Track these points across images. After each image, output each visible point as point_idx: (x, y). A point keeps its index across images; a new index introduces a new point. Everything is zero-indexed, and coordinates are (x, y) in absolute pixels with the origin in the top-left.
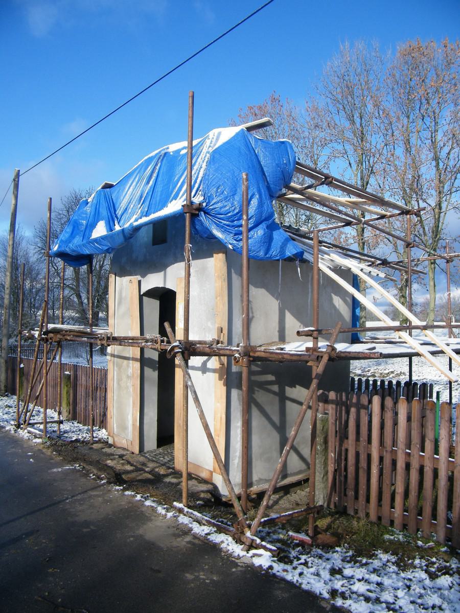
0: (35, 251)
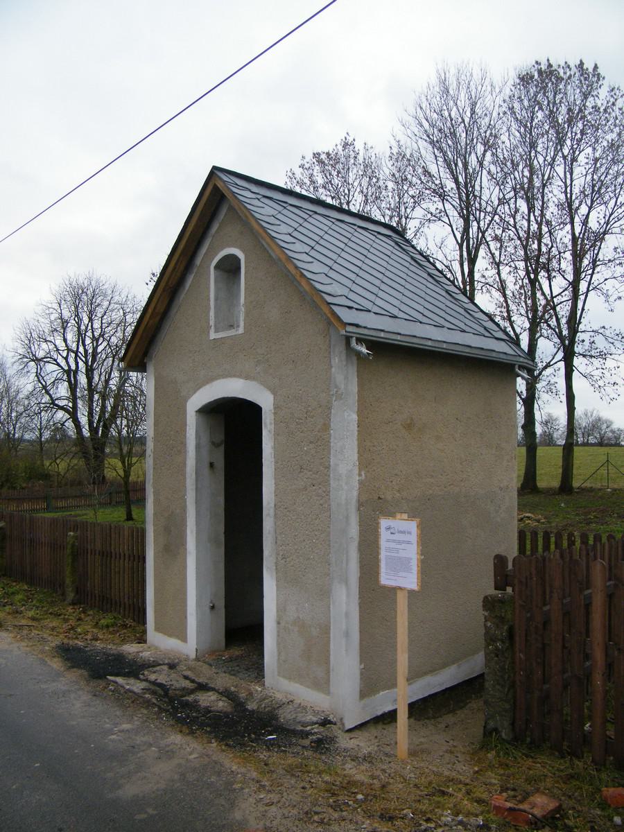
0: (14, 360)
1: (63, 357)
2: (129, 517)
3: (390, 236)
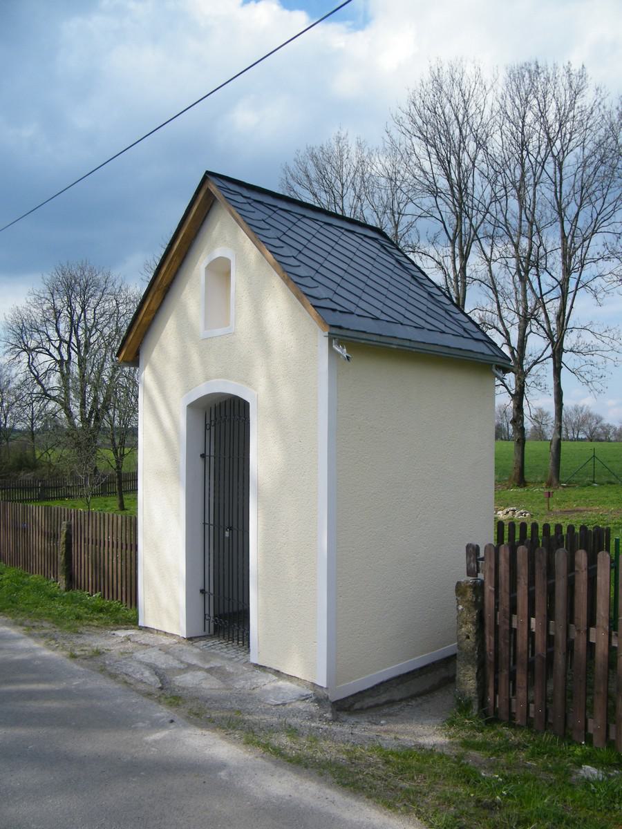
1: (55, 347)
2: (122, 507)
3: (376, 239)
